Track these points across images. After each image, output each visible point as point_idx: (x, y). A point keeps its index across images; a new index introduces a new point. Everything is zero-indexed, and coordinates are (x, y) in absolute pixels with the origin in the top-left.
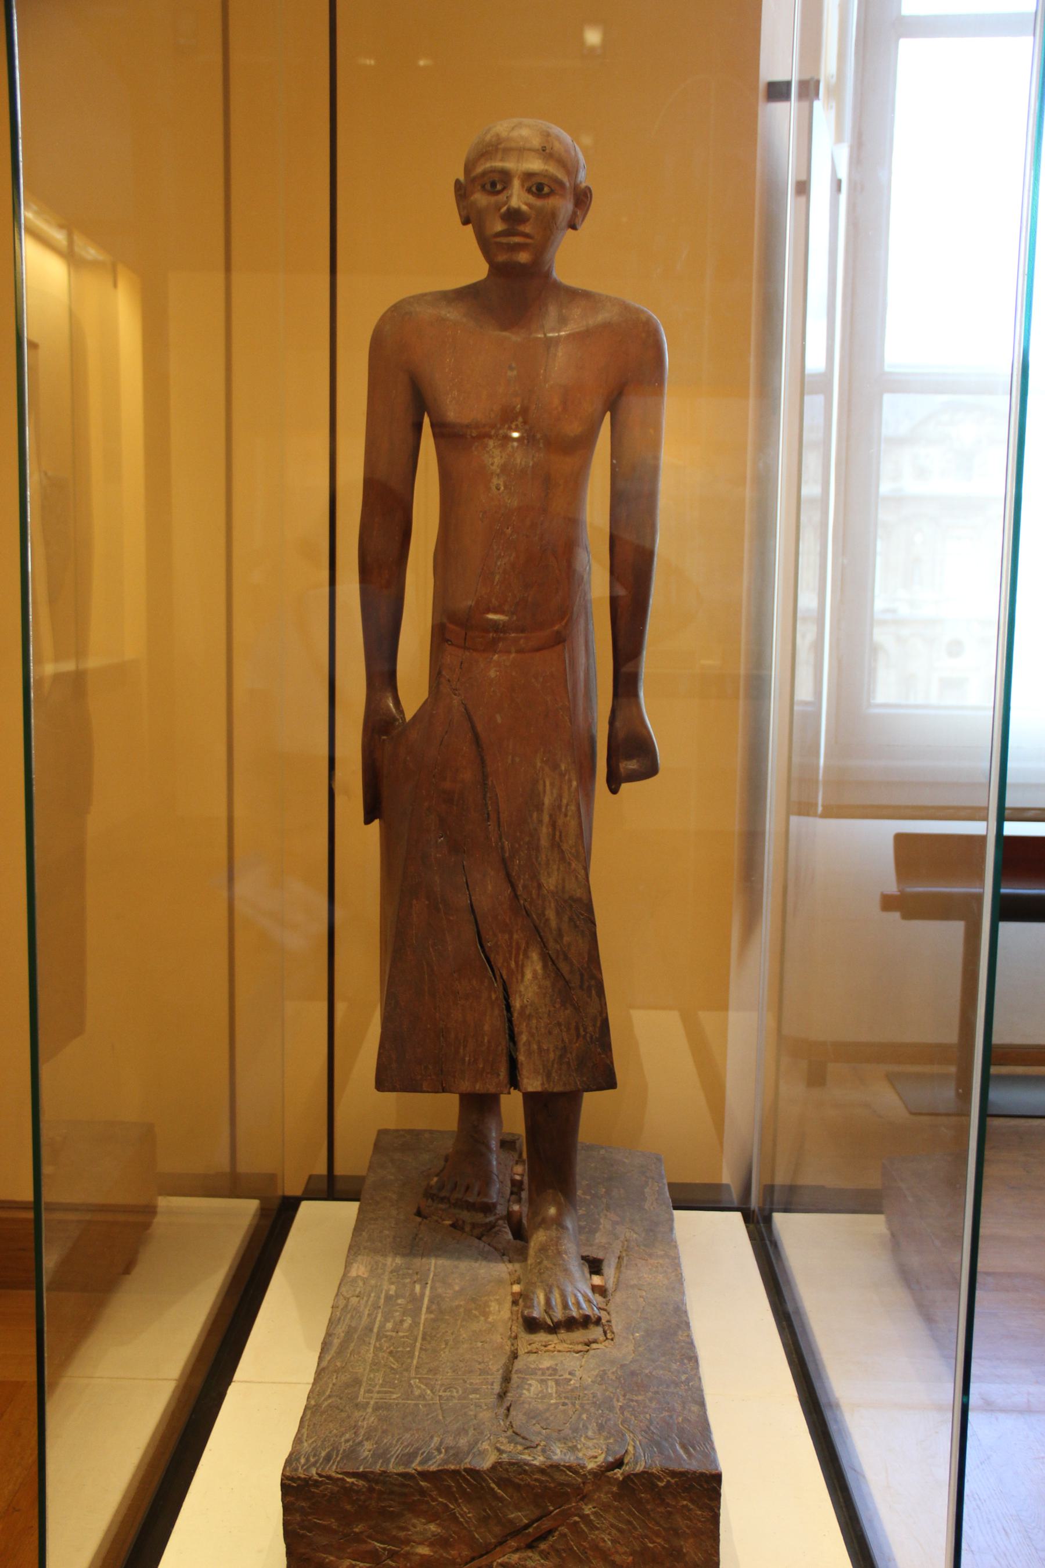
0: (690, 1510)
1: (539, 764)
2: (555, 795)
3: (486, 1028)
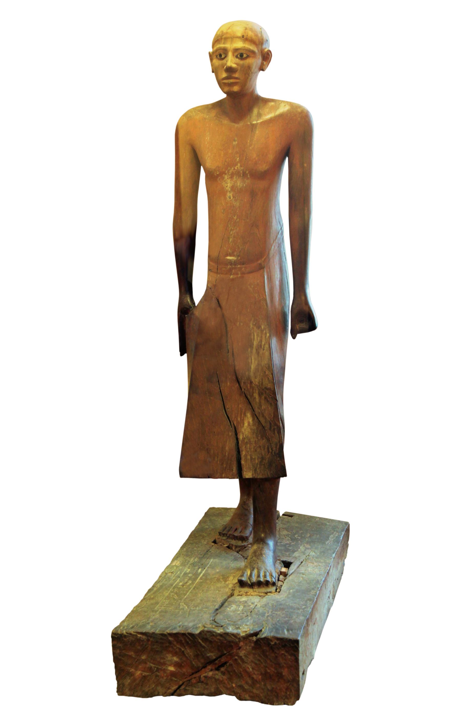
0: (285, 656)
1: (251, 326)
2: (259, 340)
3: (227, 448)
